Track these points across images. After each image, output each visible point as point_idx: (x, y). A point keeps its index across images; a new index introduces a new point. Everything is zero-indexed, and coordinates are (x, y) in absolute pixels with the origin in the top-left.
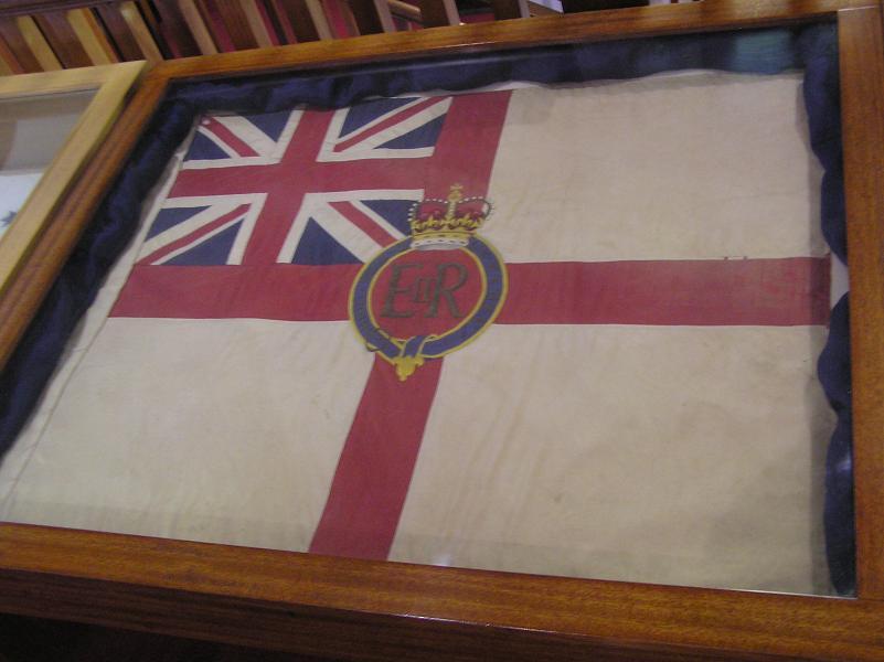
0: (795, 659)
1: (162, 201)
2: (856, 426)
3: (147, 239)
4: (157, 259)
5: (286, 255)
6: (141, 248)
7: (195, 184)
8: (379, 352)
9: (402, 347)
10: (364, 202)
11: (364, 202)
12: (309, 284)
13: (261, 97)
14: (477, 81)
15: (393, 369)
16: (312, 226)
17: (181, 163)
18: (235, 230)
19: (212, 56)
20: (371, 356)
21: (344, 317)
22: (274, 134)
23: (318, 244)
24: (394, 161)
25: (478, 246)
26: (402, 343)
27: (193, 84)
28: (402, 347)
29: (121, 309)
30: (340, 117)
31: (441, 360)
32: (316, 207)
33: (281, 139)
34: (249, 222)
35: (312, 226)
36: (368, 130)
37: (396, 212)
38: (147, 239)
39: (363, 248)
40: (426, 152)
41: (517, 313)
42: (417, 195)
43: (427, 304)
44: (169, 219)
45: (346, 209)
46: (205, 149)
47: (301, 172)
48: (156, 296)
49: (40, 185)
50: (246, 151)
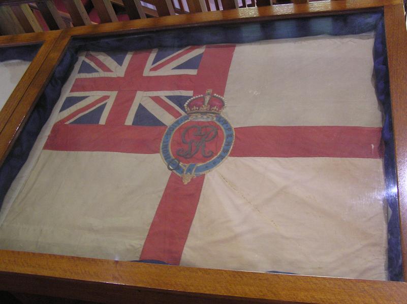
0: (93, 303)
1: (67, 92)
2: (27, 250)
3: (61, 111)
4: (68, 120)
5: (129, 121)
6: (57, 116)
7: (80, 86)
8: (175, 171)
9: (185, 169)
10: (167, 97)
11: (167, 97)
12: (143, 135)
13: (118, 45)
14: (230, 32)
15: (181, 179)
16: (141, 108)
17: (75, 75)
18: (102, 108)
19: (90, 25)
20: (170, 172)
21: (156, 151)
22: (120, 63)
23: (143, 116)
24: (180, 76)
25: (220, 119)
26: (185, 166)
27: (64, 57)
28: (185, 169)
29: (46, 147)
30: (152, 56)
31: (204, 175)
32: (142, 98)
33: (124, 63)
34: (110, 103)
35: (141, 108)
36: (73, 117)
37: (179, 101)
38: (61, 111)
39: (167, 119)
40: (193, 72)
41: (240, 152)
42: (190, 93)
43: (198, 146)
44: (71, 102)
45: (157, 100)
46: (86, 68)
47: (134, 81)
48: (63, 141)
49: (31, 65)
50: (106, 69)
